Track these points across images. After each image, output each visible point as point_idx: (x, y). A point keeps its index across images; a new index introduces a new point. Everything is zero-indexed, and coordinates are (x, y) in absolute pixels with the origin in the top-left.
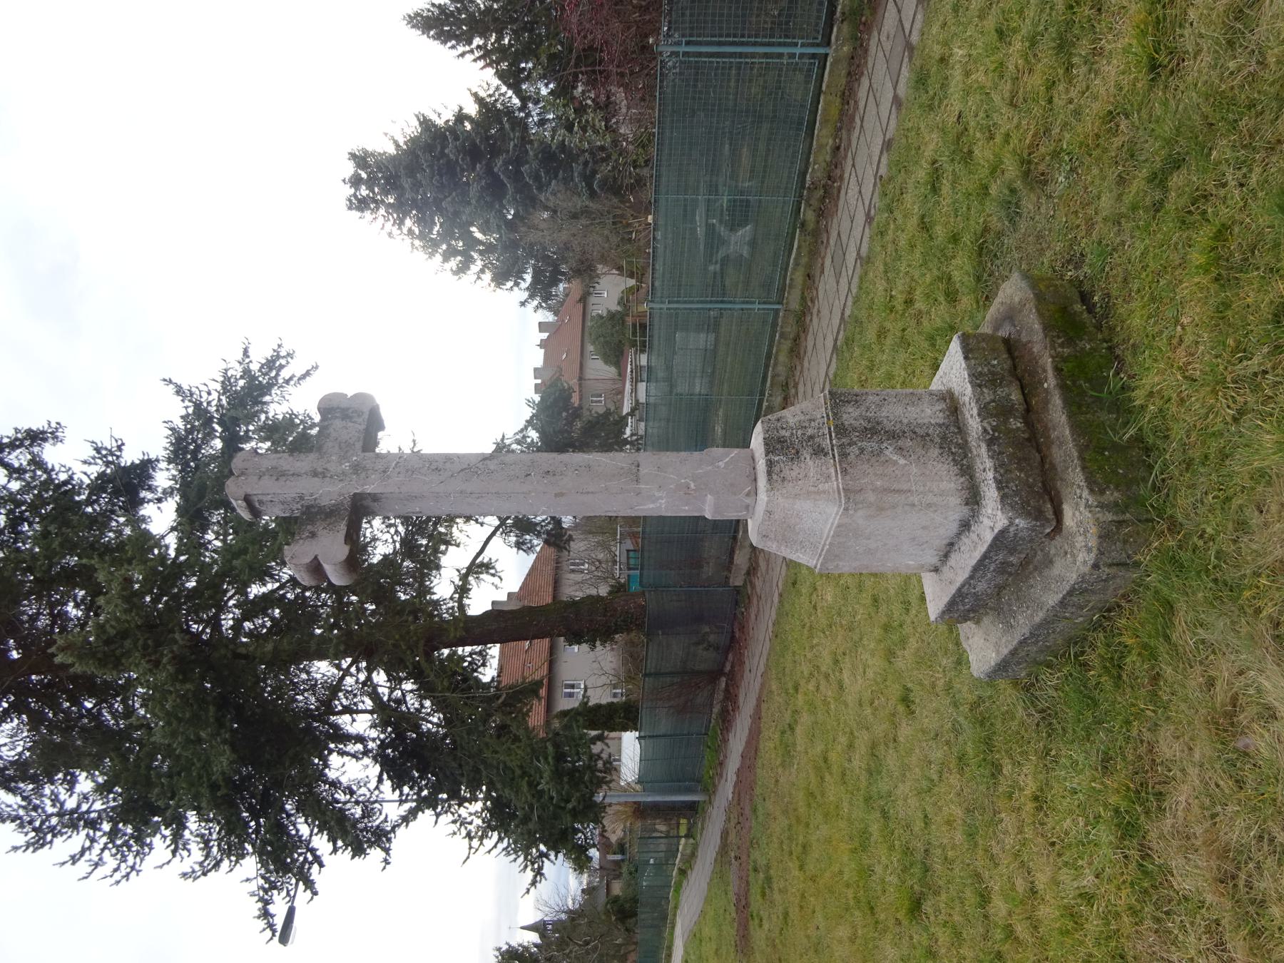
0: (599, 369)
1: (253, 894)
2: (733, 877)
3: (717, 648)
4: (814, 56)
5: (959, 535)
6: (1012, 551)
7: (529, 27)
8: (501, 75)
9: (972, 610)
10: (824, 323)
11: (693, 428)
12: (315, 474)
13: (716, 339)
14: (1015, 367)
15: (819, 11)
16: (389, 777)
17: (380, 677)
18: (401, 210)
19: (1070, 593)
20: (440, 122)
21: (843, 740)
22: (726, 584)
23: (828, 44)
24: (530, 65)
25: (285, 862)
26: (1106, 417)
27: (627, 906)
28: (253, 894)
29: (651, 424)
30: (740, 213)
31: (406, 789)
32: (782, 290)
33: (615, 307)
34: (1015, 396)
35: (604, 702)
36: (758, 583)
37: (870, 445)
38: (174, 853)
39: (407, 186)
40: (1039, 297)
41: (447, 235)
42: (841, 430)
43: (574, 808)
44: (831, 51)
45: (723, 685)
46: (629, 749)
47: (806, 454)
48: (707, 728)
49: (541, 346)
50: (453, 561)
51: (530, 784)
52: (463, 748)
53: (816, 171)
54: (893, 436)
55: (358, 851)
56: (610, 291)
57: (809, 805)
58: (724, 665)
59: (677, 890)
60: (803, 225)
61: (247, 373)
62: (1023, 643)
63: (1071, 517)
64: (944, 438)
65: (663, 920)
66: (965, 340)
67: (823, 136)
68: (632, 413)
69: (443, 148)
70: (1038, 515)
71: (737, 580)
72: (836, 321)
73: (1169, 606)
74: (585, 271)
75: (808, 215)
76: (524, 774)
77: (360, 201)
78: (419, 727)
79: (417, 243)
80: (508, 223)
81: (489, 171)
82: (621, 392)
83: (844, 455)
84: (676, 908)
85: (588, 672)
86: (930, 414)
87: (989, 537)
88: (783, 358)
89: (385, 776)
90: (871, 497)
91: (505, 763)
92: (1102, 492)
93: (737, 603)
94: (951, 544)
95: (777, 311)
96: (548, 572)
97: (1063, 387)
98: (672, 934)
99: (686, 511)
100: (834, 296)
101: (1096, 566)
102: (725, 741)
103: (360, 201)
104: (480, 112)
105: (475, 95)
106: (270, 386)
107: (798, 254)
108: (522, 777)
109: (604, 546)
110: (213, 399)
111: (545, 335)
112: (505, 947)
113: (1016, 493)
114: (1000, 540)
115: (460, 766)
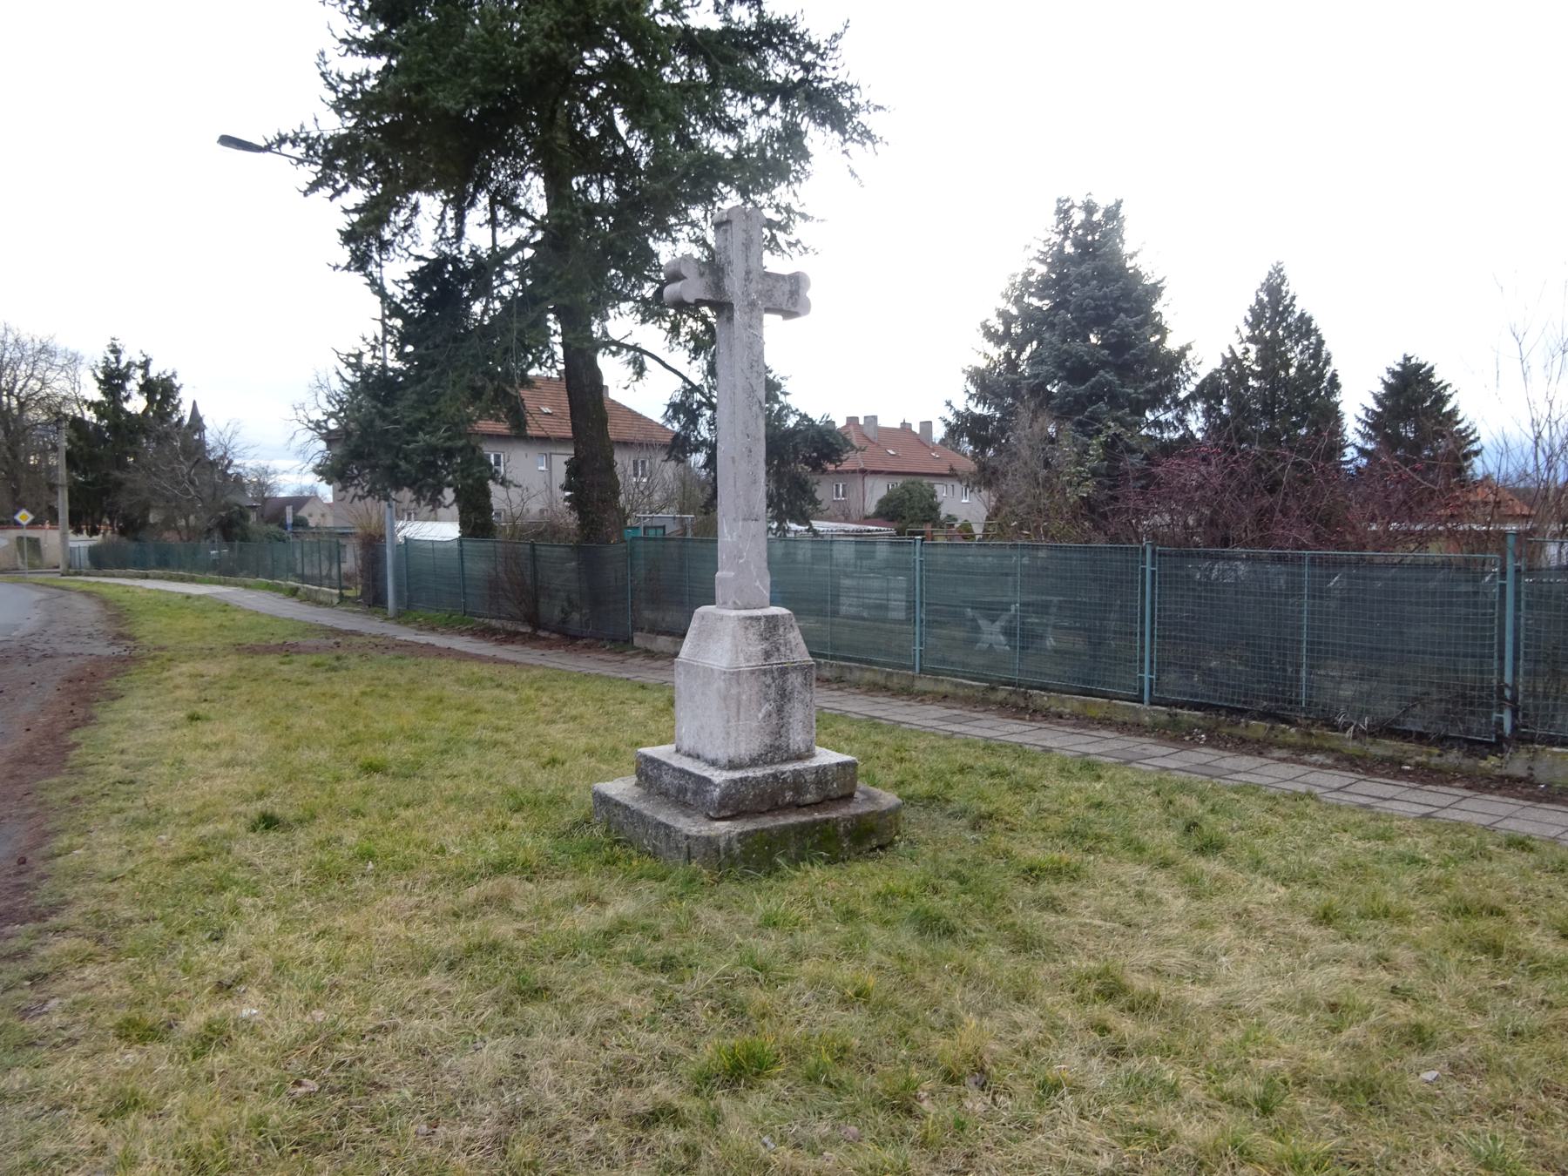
0: (876, 491)
1: (302, 127)
2: (312, 641)
3: (564, 621)
4: (1142, 691)
5: (706, 761)
6: (695, 793)
7: (1268, 412)
8: (1212, 379)
9: (647, 777)
10: (898, 710)
11: (800, 588)
12: (748, 273)
13: (901, 622)
14: (832, 800)
15: (1179, 693)
16: (422, 269)
17: (528, 253)
18: (1059, 260)
19: (667, 827)
20: (1157, 307)
21: (502, 723)
22: (636, 628)
23: (1152, 704)
24: (1224, 411)
25: (335, 159)
26: (793, 850)
27: (237, 530)
28: (302, 127)
29: (808, 546)
30: (1022, 637)
31: (410, 286)
32: (935, 672)
33: (944, 512)
34: (809, 798)
35: (493, 500)
36: (637, 661)
37: (772, 692)
38: (344, 41)
39: (1083, 268)
40: (882, 815)
41: (1028, 315)
42: (784, 672)
43: (398, 466)
44: (1146, 706)
45: (523, 630)
46: (444, 530)
47: (765, 645)
48: (473, 614)
49: (904, 423)
50: (652, 336)
51: (422, 421)
52: (457, 349)
53: (1042, 699)
54: (780, 710)
55: (348, 237)
56: (963, 505)
57: (428, 699)
58: (545, 629)
59: (268, 587)
60: (993, 689)
61: (856, 108)
62: (627, 807)
63: (722, 827)
64: (778, 748)
65: (226, 572)
66: (853, 765)
67: (1073, 703)
68: (811, 529)
69: (1126, 311)
70: (722, 805)
71: (639, 640)
72: (898, 718)
73: (663, 878)
74: (985, 477)
75: (1002, 694)
76: (432, 415)
77: (1067, 212)
78: (476, 299)
79: (1019, 279)
80: (1042, 386)
81: (1104, 364)
82: (847, 520)
83: (765, 673)
84: (246, 586)
85: (531, 482)
86: (797, 739)
87: (706, 774)
88: (868, 676)
89: (423, 264)
90: (734, 691)
91: (443, 394)
92: (739, 841)
93: (614, 641)
94: (698, 757)
95: (913, 668)
96: (643, 437)
97: (815, 823)
98: (211, 582)
99: (722, 556)
100: (925, 716)
101: (688, 837)
102: (461, 633)
103: (1067, 212)
104: (1169, 352)
105: (1189, 347)
106: (843, 132)
107: (966, 686)
108: (429, 413)
109: (667, 502)
110: (831, 72)
111: (916, 429)
112: (176, 382)
113: (738, 791)
114: (708, 781)
115: (436, 346)
